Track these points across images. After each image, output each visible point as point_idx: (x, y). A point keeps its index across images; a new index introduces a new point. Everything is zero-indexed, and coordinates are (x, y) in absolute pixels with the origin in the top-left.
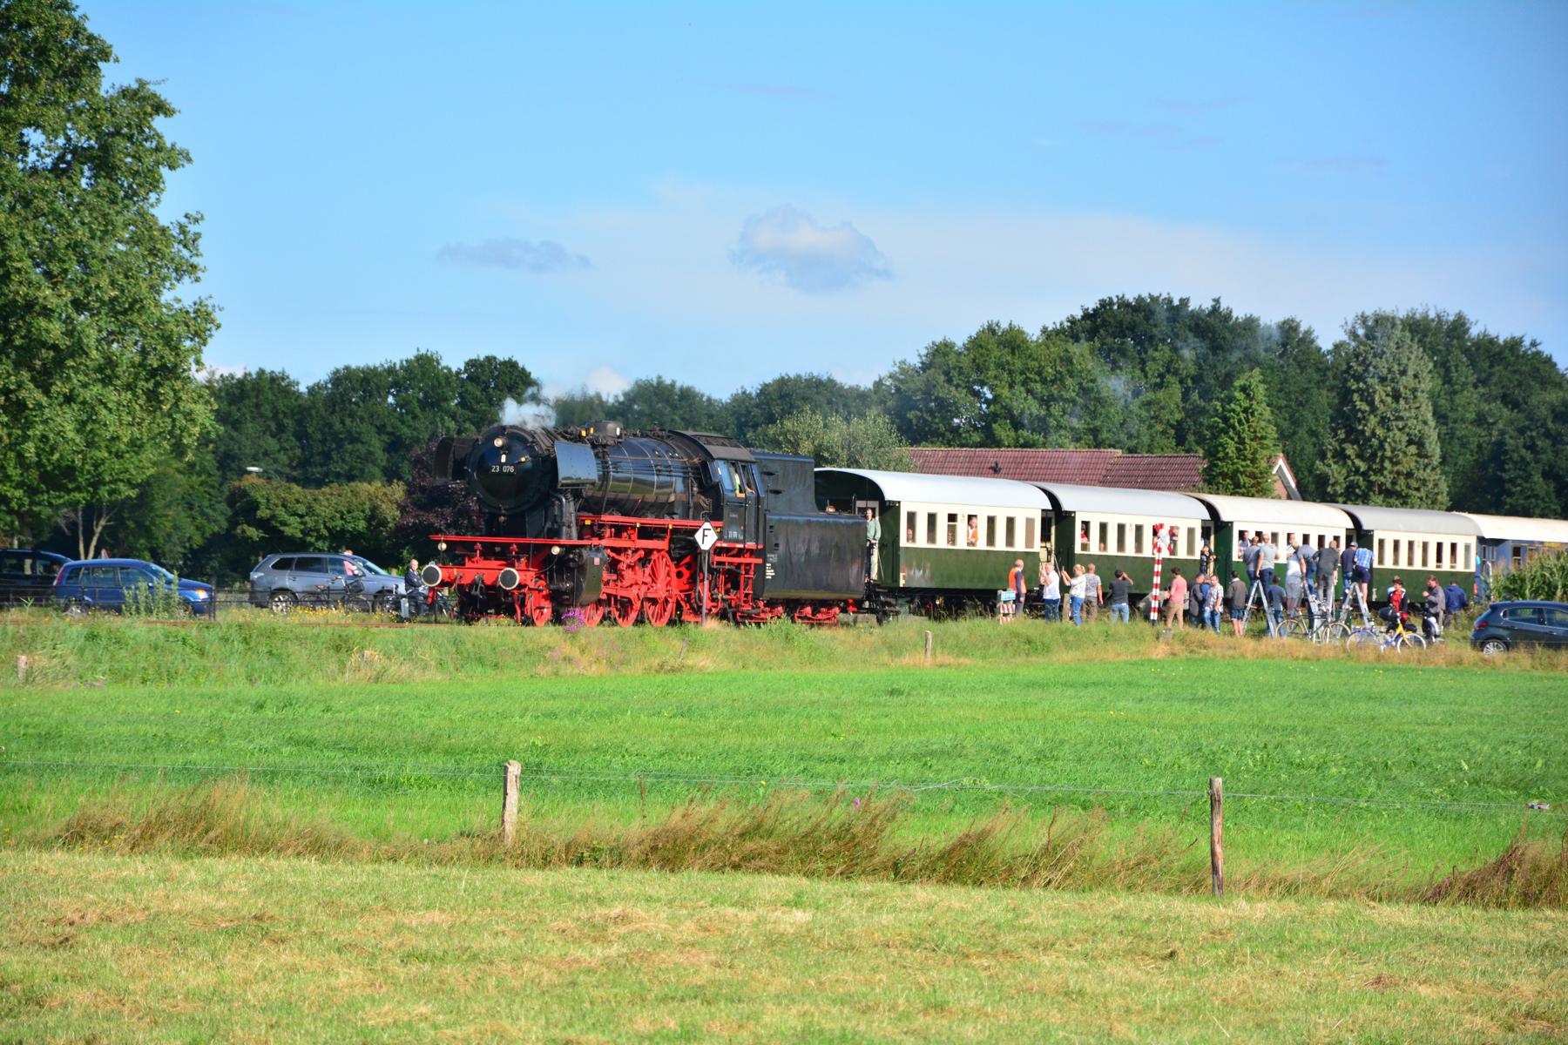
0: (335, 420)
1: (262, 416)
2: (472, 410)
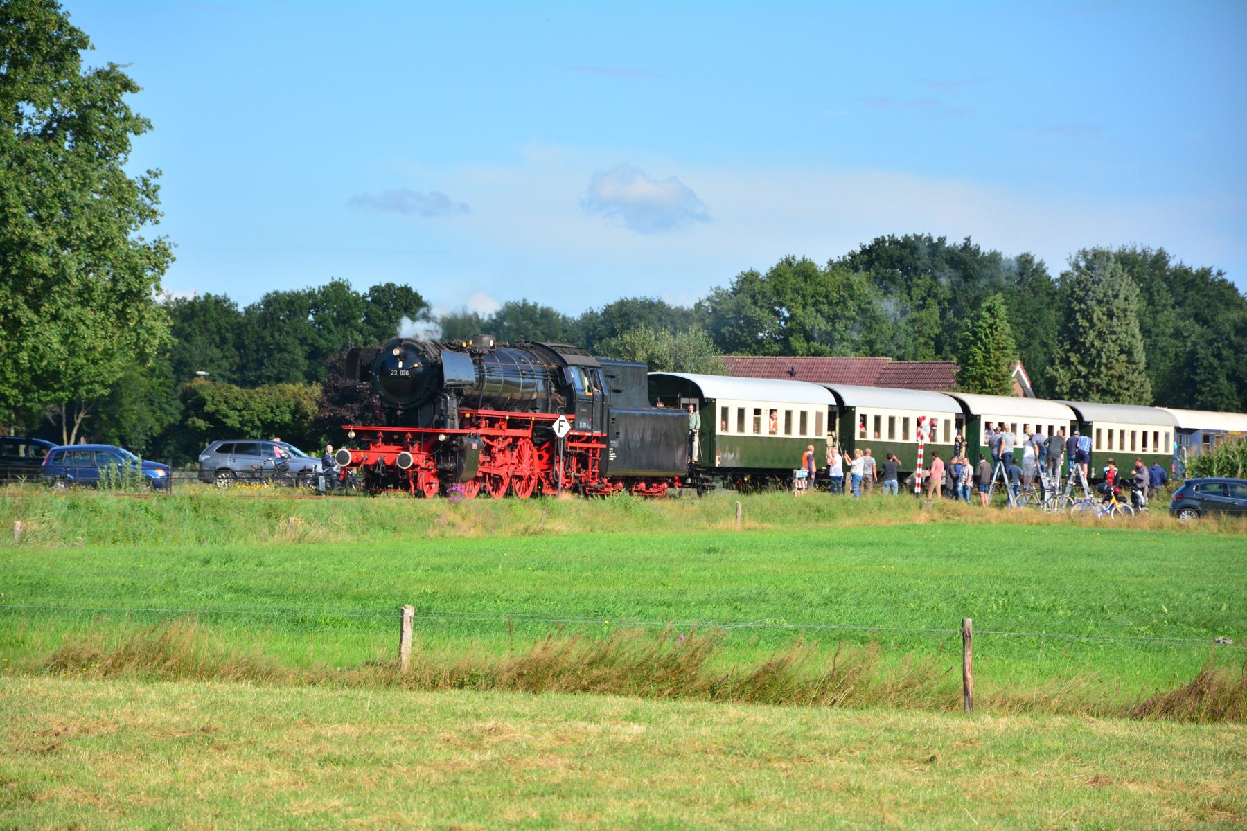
0: (267, 334)
1: (208, 331)
2: (376, 326)
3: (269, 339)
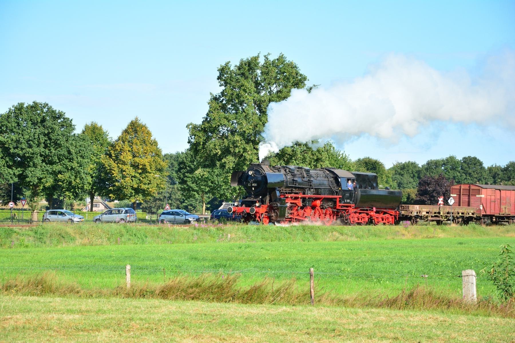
0: (428, 173)
1: (409, 173)
2: (464, 170)
3: (428, 175)
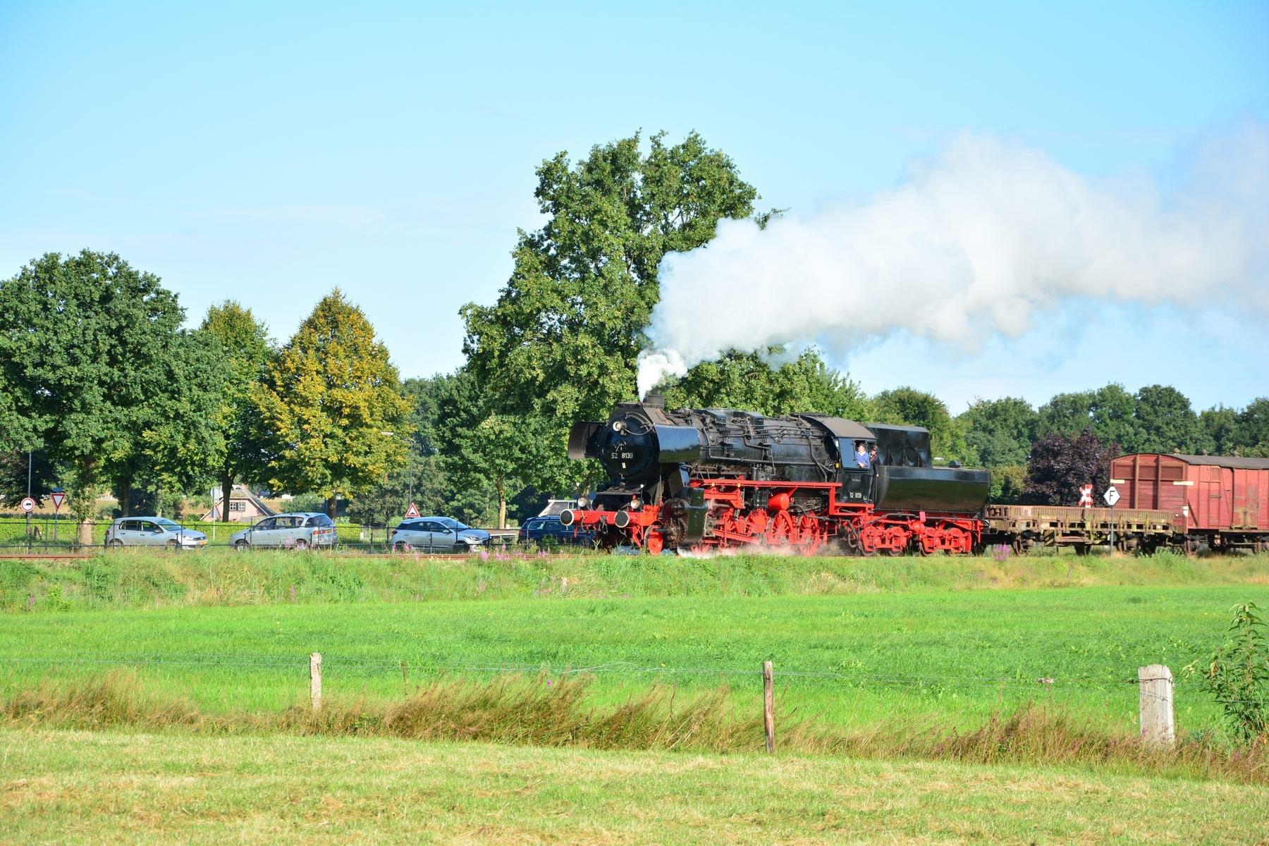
0: (1054, 428)
1: (1007, 426)
2: (1144, 420)
3: (1056, 432)
